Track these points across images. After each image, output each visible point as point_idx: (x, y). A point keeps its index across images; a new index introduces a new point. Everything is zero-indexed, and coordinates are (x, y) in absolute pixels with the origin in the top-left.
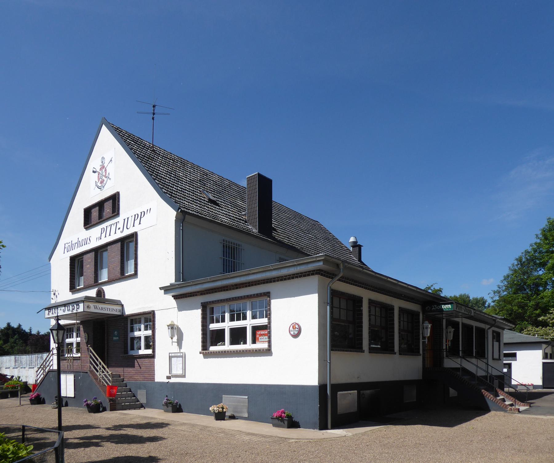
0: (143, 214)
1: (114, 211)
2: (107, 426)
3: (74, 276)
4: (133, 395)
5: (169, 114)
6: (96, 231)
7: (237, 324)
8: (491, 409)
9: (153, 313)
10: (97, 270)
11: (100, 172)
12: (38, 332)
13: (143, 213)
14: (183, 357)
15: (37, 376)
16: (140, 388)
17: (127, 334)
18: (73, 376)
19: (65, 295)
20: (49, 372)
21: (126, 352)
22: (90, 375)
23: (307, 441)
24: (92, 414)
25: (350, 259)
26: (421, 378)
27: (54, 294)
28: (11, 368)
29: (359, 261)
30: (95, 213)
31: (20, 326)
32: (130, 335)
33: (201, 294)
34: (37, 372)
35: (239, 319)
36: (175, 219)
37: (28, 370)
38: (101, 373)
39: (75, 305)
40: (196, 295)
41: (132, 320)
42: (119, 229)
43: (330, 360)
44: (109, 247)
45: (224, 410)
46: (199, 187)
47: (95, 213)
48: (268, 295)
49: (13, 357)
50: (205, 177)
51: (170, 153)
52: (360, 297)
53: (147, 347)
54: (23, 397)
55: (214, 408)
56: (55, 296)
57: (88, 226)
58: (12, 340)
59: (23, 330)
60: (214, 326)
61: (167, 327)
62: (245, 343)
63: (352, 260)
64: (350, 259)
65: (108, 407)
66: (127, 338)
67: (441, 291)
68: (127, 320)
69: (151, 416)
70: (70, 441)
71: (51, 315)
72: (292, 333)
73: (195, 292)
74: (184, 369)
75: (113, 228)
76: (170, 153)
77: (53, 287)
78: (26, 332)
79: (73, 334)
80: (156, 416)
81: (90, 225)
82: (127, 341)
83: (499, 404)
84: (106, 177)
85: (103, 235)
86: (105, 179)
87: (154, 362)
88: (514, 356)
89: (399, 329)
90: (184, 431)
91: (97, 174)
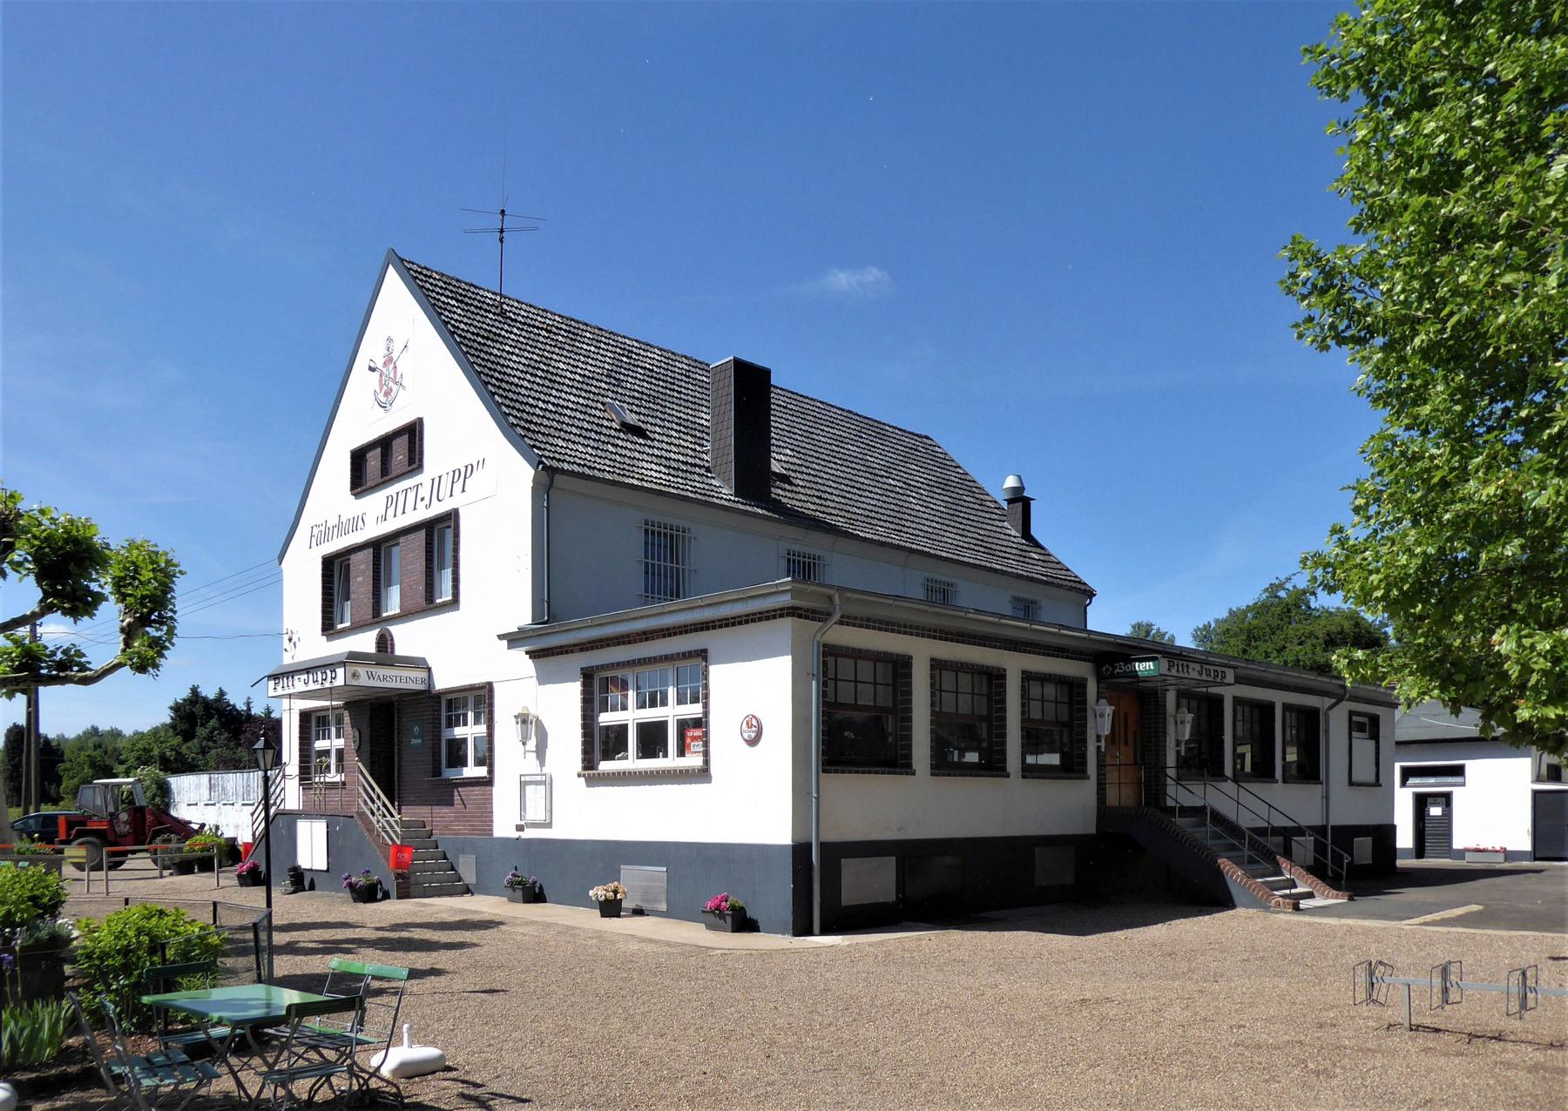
0: (470, 469)
1: (411, 461)
2: (378, 925)
3: (332, 600)
4: (449, 866)
5: (536, 229)
6: (375, 502)
7: (651, 714)
8: (1236, 902)
9: (488, 689)
10: (379, 588)
11: (384, 370)
12: (268, 709)
13: (469, 468)
14: (548, 783)
15: (253, 824)
16: (463, 852)
17: (440, 732)
18: (325, 825)
19: (311, 644)
20: (276, 815)
21: (437, 772)
22: (359, 822)
23: (744, 952)
24: (361, 905)
25: (997, 535)
26: (1092, 830)
27: (290, 640)
28: (201, 804)
29: (1023, 537)
30: (373, 461)
31: (222, 693)
32: (446, 734)
33: (582, 650)
34: (252, 814)
35: (653, 704)
36: (531, 484)
37: (241, 810)
38: (380, 818)
39: (328, 671)
40: (572, 652)
41: (450, 702)
42: (422, 499)
43: (818, 793)
44: (402, 540)
45: (619, 896)
46: (603, 392)
47: (373, 461)
48: (703, 654)
49: (204, 778)
50: (627, 352)
51: (543, 311)
52: (904, 656)
53: (480, 762)
54: (224, 872)
55: (598, 892)
56: (292, 644)
57: (359, 489)
58: (201, 732)
59: (230, 705)
60: (606, 718)
61: (514, 720)
63: (1002, 536)
64: (997, 535)
65: (394, 893)
66: (440, 740)
68: (440, 702)
69: (474, 909)
70: (302, 945)
71: (280, 692)
72: (746, 736)
73: (569, 646)
74: (550, 810)
75: (411, 495)
76: (543, 311)
77: (288, 623)
78: (237, 710)
80: (485, 909)
81: (364, 488)
82: (440, 748)
83: (1254, 891)
84: (396, 383)
85: (391, 511)
86: (395, 388)
87: (491, 795)
88: (1459, 771)
90: (524, 935)
91: (377, 374)
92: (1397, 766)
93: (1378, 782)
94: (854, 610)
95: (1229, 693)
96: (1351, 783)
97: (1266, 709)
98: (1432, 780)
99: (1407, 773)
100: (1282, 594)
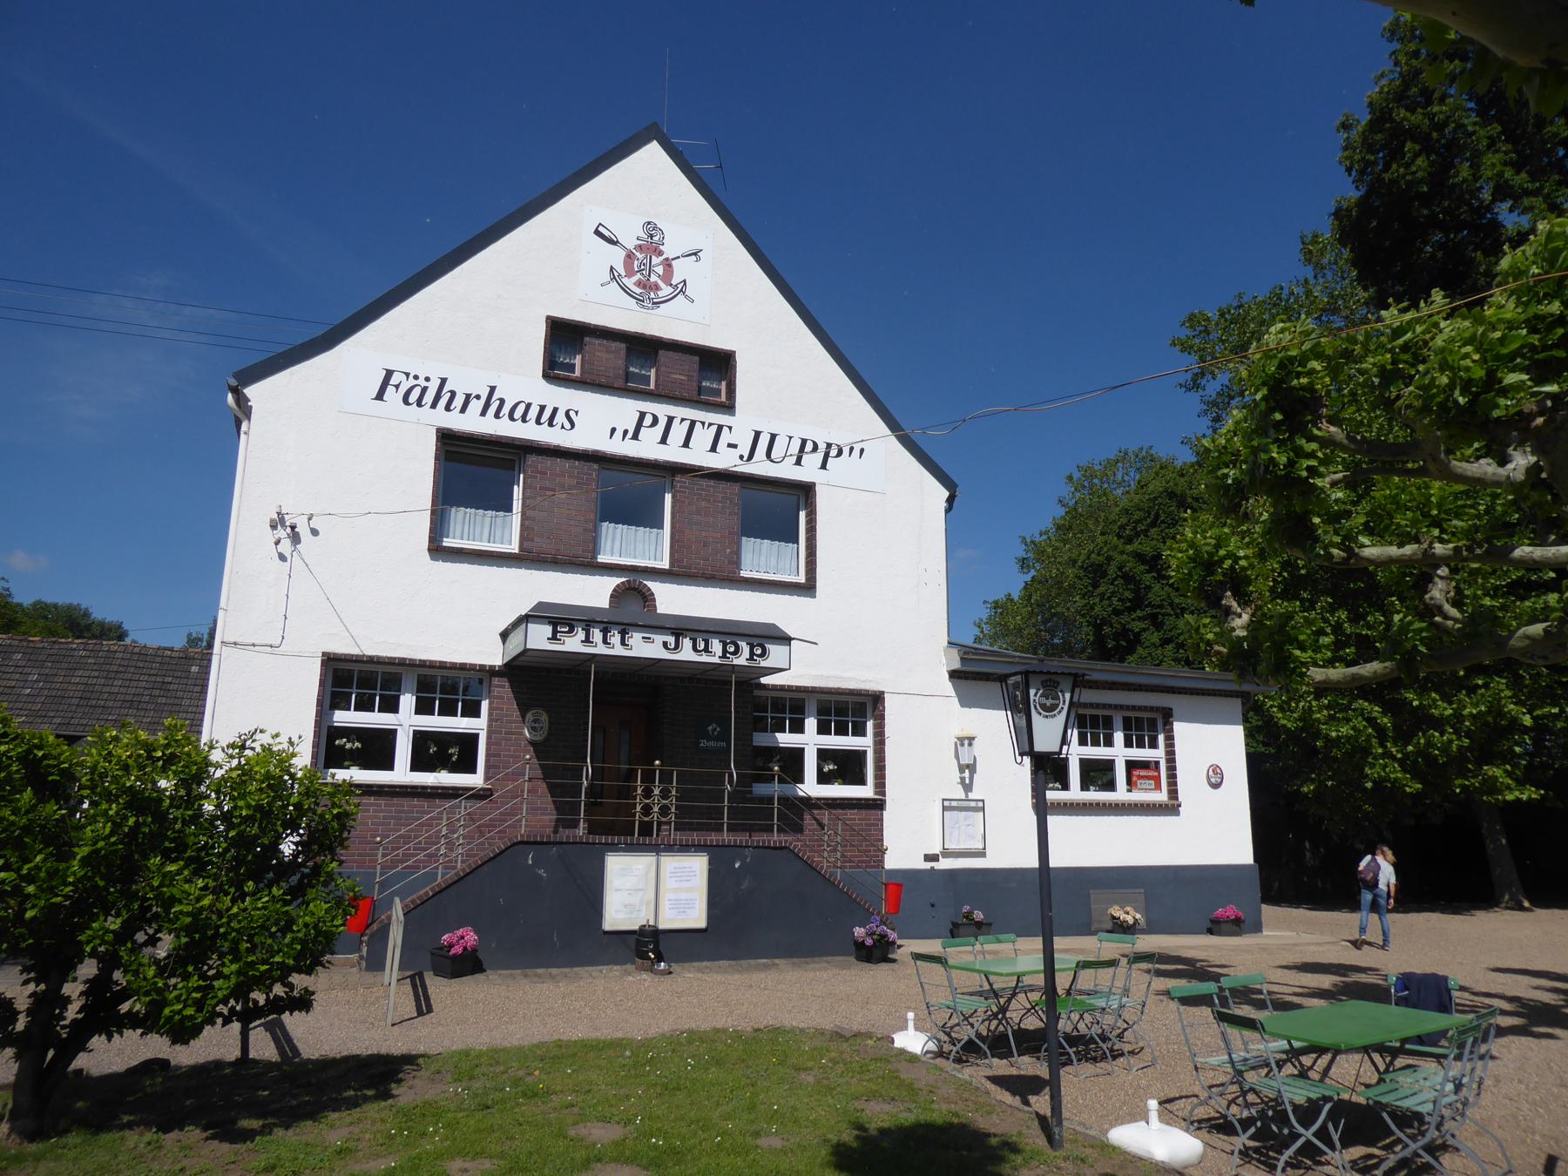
79: (864, 724)
87: (882, 820)
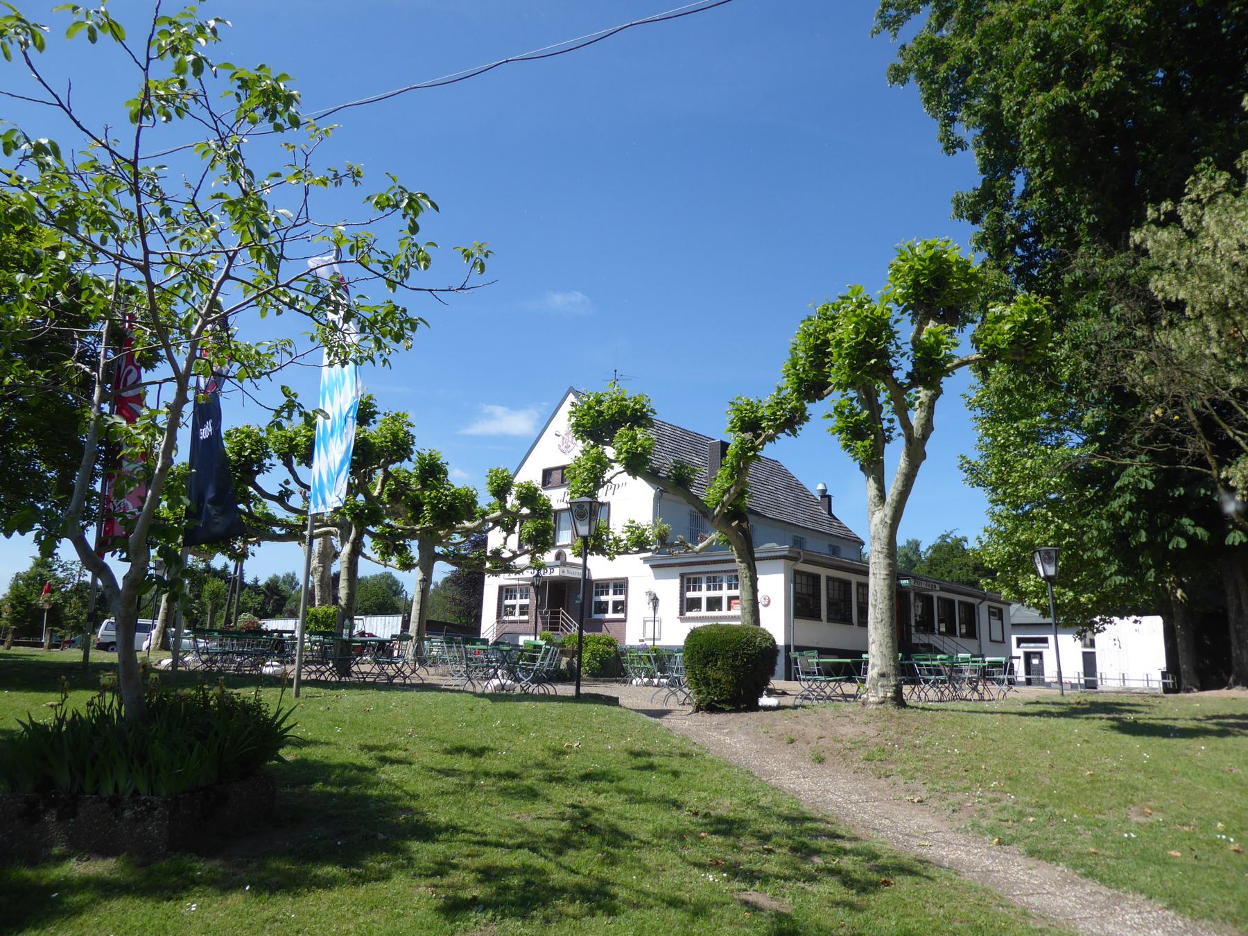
7: (714, 594)
30: (556, 476)
32: (596, 599)
35: (715, 589)
60: (690, 595)
62: (720, 609)
67: (966, 541)
89: (858, 602)
91: (561, 438)
92: (1014, 639)
93: (1004, 641)
94: (809, 558)
95: (935, 595)
96: (991, 641)
97: (951, 602)
98: (1032, 645)
99: (1020, 641)
100: (949, 540)
